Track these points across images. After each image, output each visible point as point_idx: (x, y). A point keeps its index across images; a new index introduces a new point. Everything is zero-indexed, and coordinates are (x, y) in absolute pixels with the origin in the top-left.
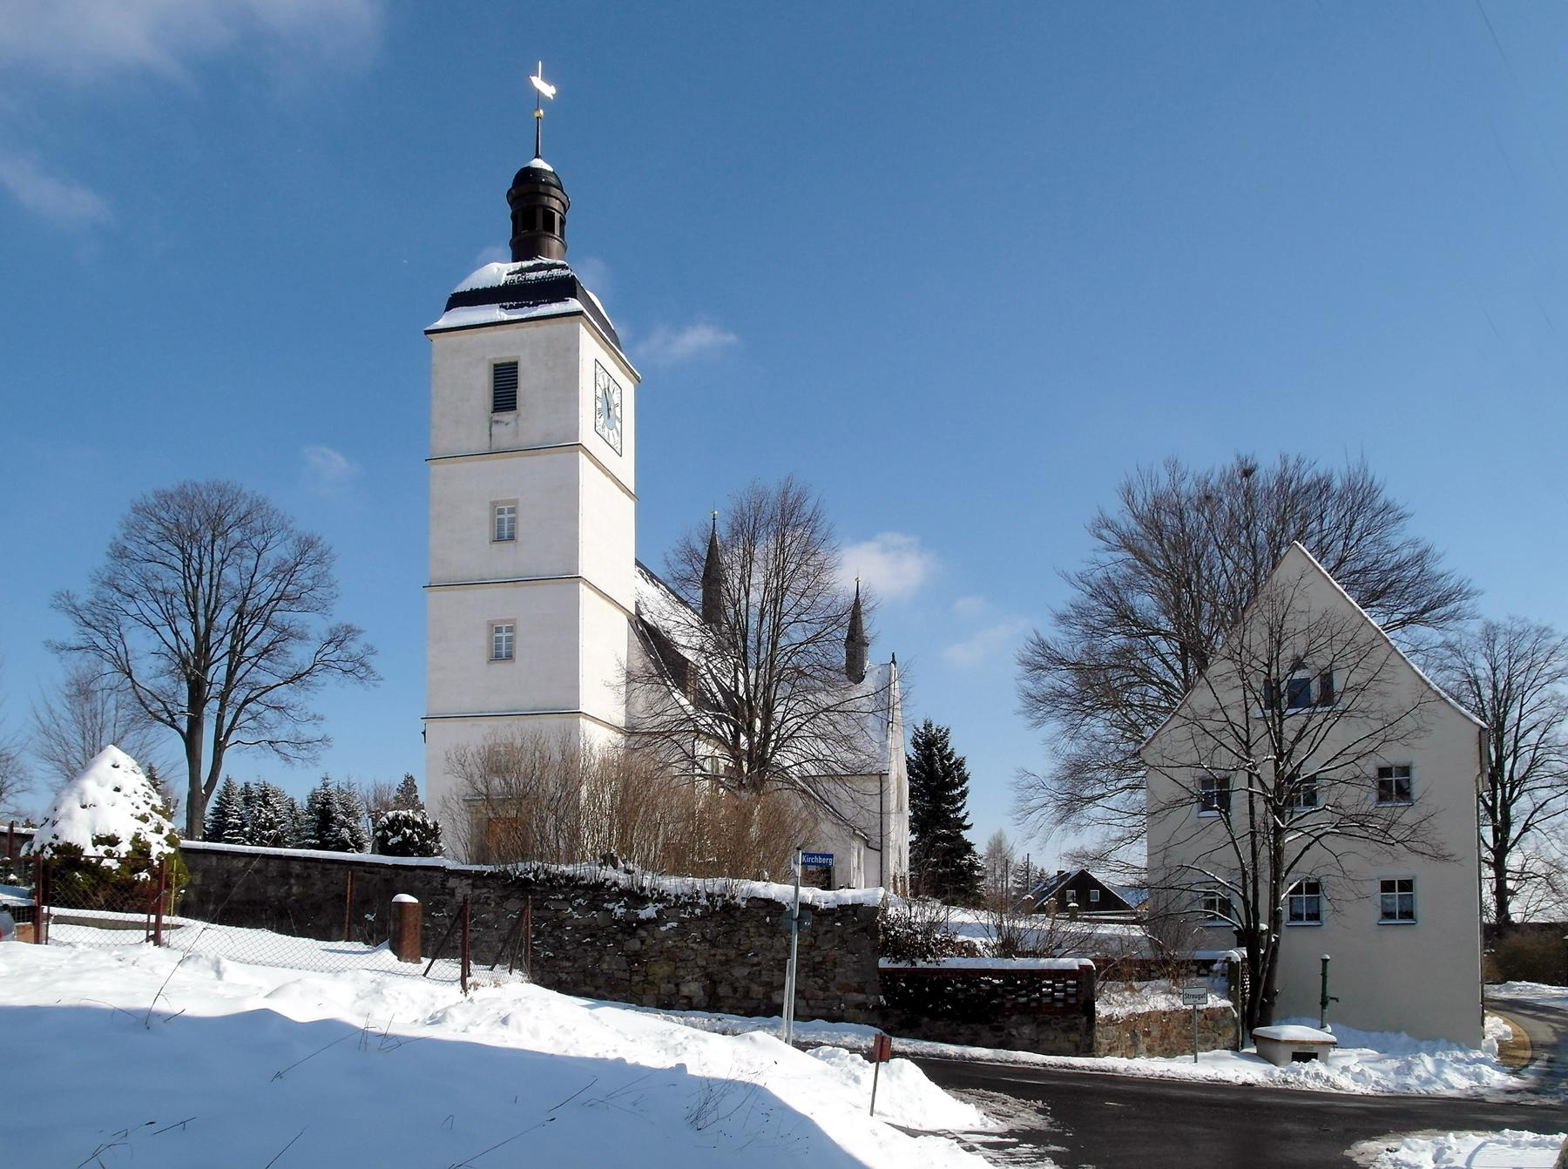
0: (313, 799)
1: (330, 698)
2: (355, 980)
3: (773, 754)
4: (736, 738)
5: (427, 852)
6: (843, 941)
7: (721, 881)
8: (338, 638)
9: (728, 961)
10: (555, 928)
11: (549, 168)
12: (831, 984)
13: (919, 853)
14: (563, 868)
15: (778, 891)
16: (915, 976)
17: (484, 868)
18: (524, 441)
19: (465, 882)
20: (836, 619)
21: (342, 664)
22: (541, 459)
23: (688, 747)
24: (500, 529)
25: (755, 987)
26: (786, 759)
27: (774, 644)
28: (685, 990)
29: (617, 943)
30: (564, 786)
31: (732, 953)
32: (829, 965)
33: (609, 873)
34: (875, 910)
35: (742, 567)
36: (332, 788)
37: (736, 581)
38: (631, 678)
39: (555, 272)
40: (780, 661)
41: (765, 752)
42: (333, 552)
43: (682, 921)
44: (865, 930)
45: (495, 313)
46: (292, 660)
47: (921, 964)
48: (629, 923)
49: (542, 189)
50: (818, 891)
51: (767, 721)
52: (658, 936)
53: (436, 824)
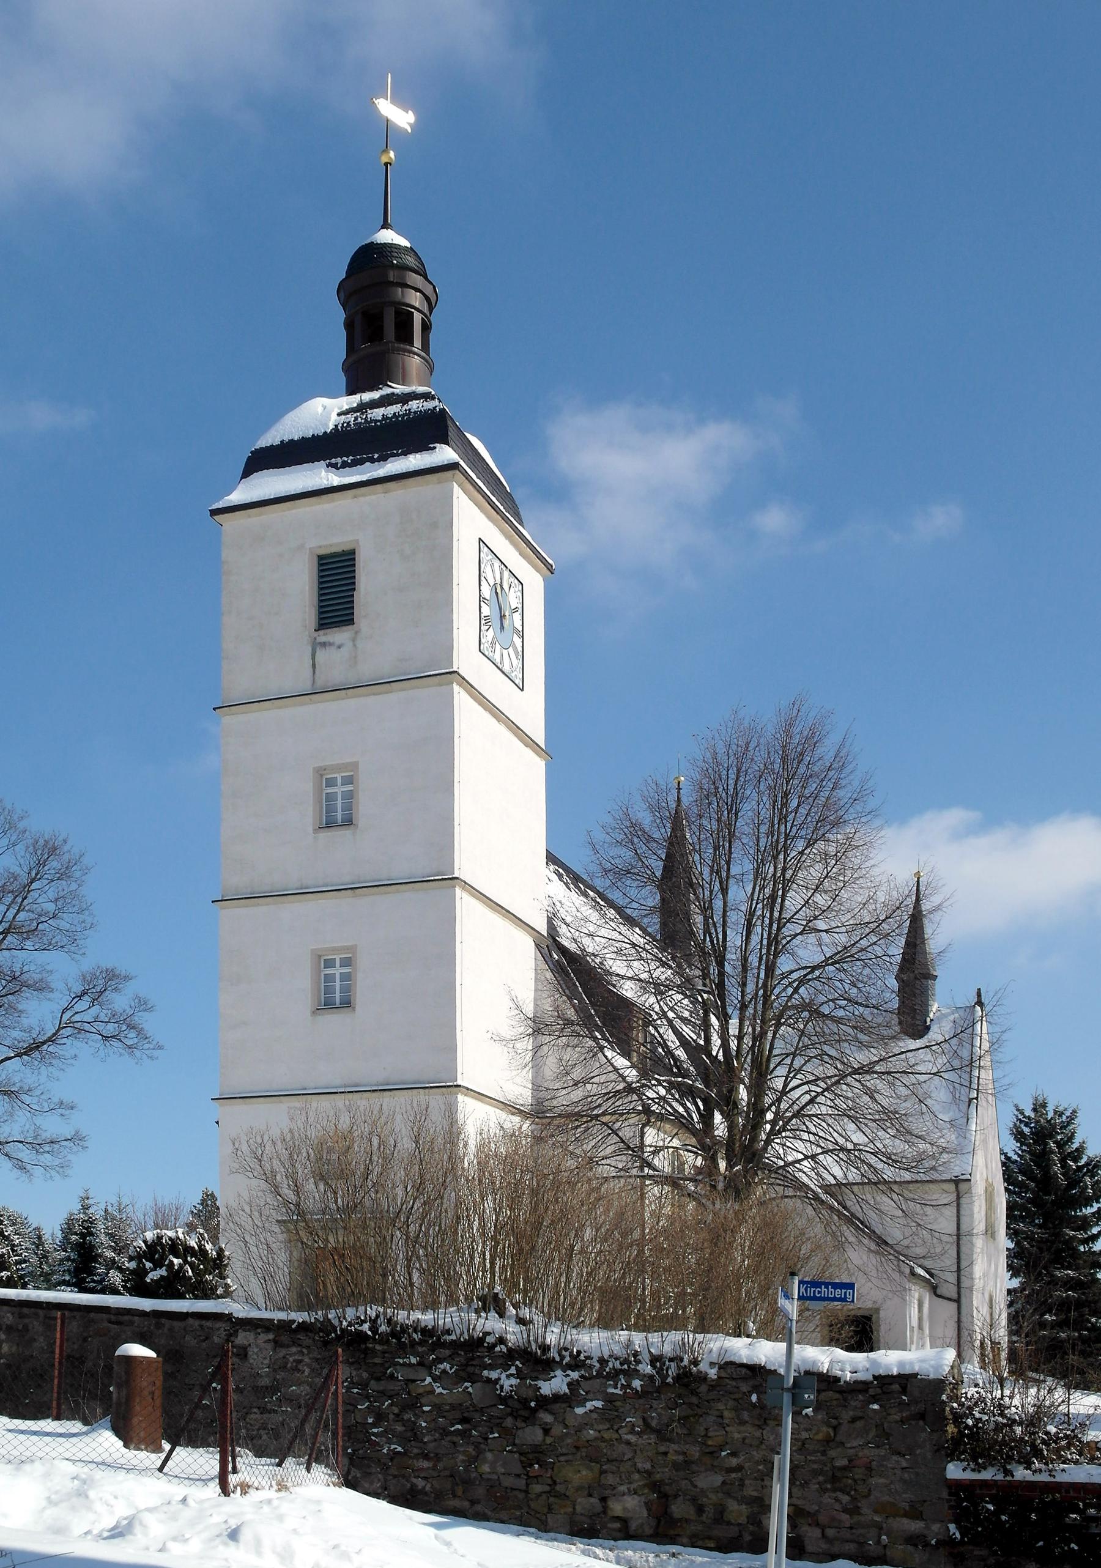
0: (68, 1229)
1: (83, 1076)
2: (47, 1475)
3: (768, 1142)
4: (707, 1118)
5: (204, 1292)
6: (884, 1434)
7: (675, 1336)
8: (97, 987)
9: (688, 1463)
10: (404, 1408)
11: (404, 242)
12: (863, 1504)
13: (1023, 1308)
14: (416, 1315)
15: (767, 1352)
16: (1010, 1494)
17: (293, 1315)
18: (367, 670)
19: (263, 1337)
20: (876, 927)
21: (101, 1027)
22: (394, 698)
23: (627, 1133)
24: (330, 810)
25: (733, 1506)
26: (790, 1150)
27: (770, 969)
28: (617, 1508)
29: (506, 1433)
30: (419, 1188)
31: (695, 1451)
32: (859, 1473)
33: (491, 1324)
34: (939, 1385)
35: (716, 848)
36: (96, 1212)
37: (706, 871)
38: (538, 1027)
39: (414, 405)
40: (781, 994)
41: (754, 1139)
42: (86, 861)
43: (610, 1400)
44: (922, 1416)
45: (320, 475)
46: (25, 1022)
47: (1021, 1473)
48: (524, 1402)
49: (392, 276)
50: (840, 1353)
51: (758, 1087)
52: (570, 1421)
53: (220, 1252)
